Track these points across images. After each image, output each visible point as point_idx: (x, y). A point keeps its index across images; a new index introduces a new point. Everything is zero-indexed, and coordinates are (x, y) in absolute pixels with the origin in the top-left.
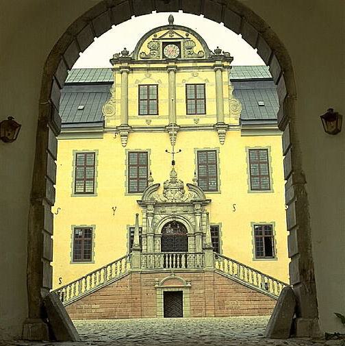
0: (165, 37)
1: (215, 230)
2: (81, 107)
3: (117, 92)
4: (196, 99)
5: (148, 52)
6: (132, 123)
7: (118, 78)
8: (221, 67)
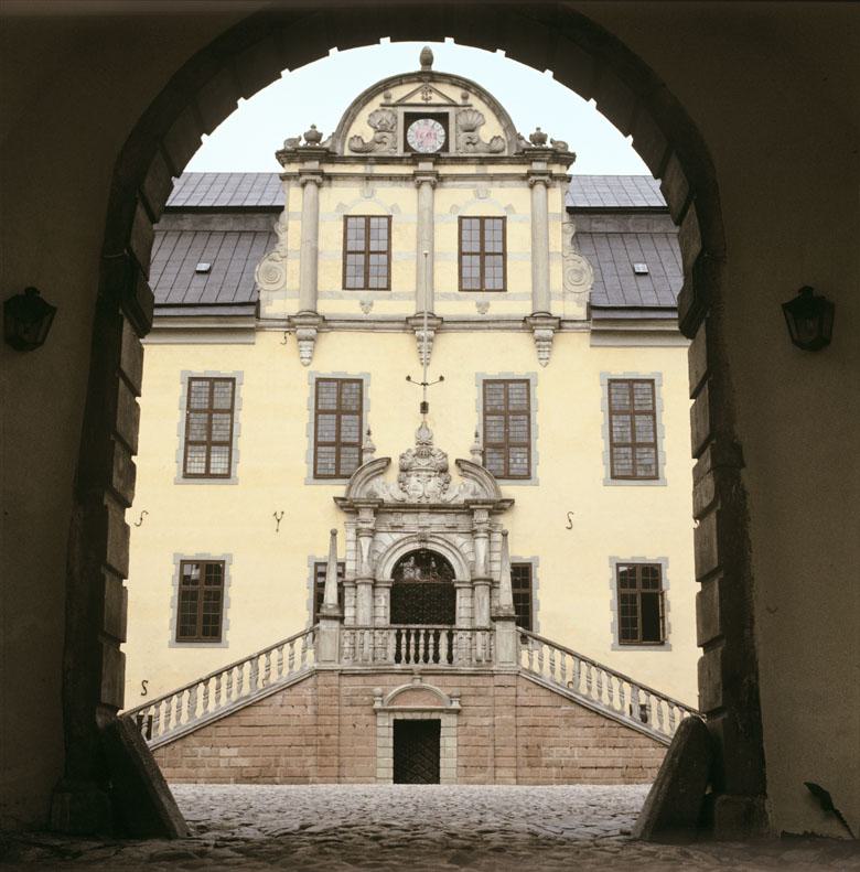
1: (522, 575)
2: (203, 267)
4: (483, 252)
5: (369, 135)
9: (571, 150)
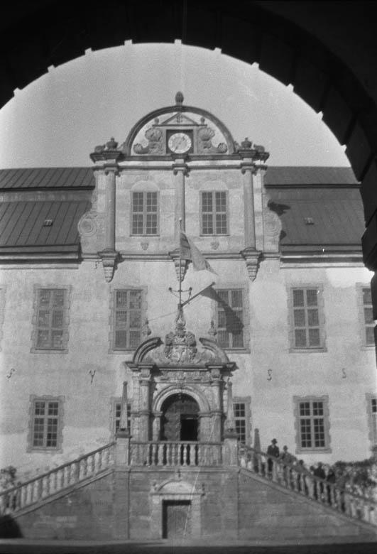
0: (170, 123)
3: (101, 201)
6: (120, 247)
7: (102, 181)
8: (252, 167)
9: (266, 151)
